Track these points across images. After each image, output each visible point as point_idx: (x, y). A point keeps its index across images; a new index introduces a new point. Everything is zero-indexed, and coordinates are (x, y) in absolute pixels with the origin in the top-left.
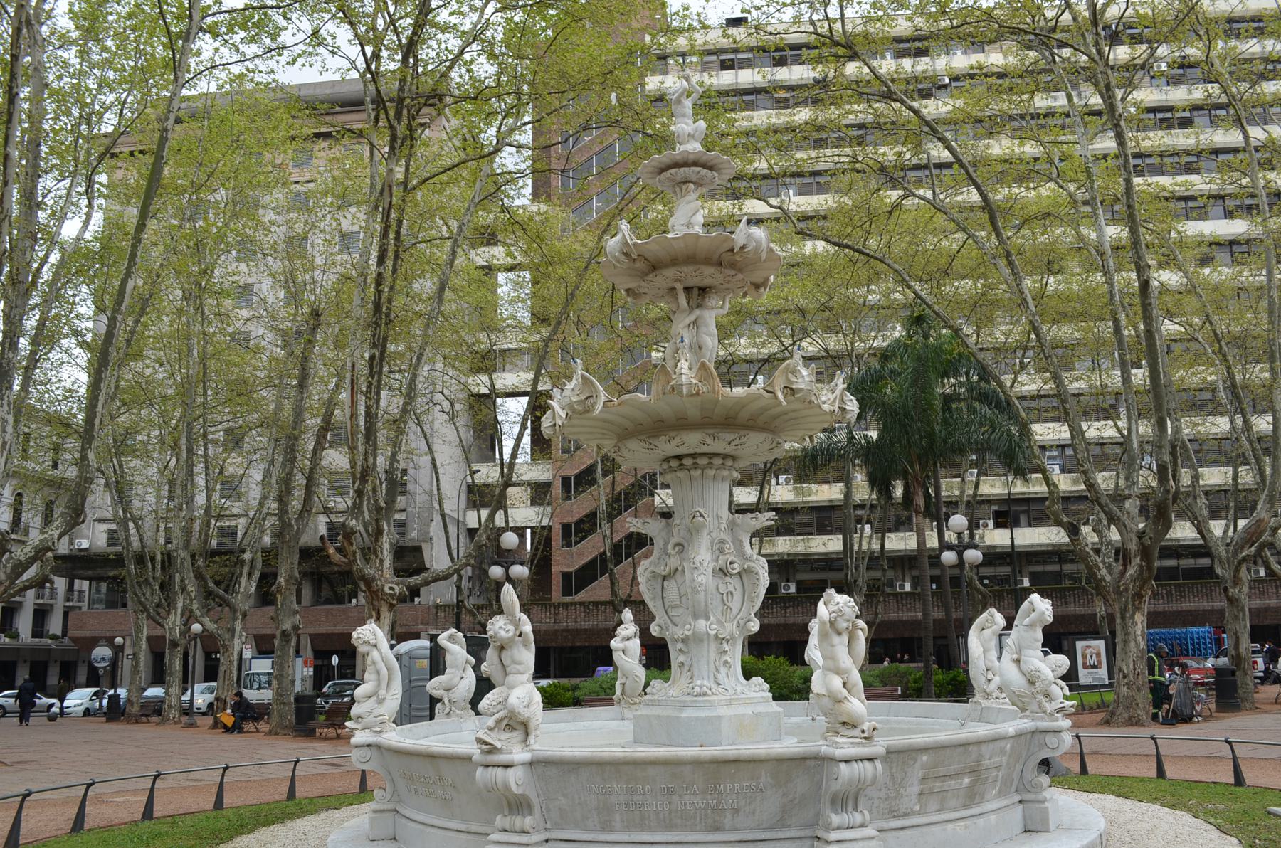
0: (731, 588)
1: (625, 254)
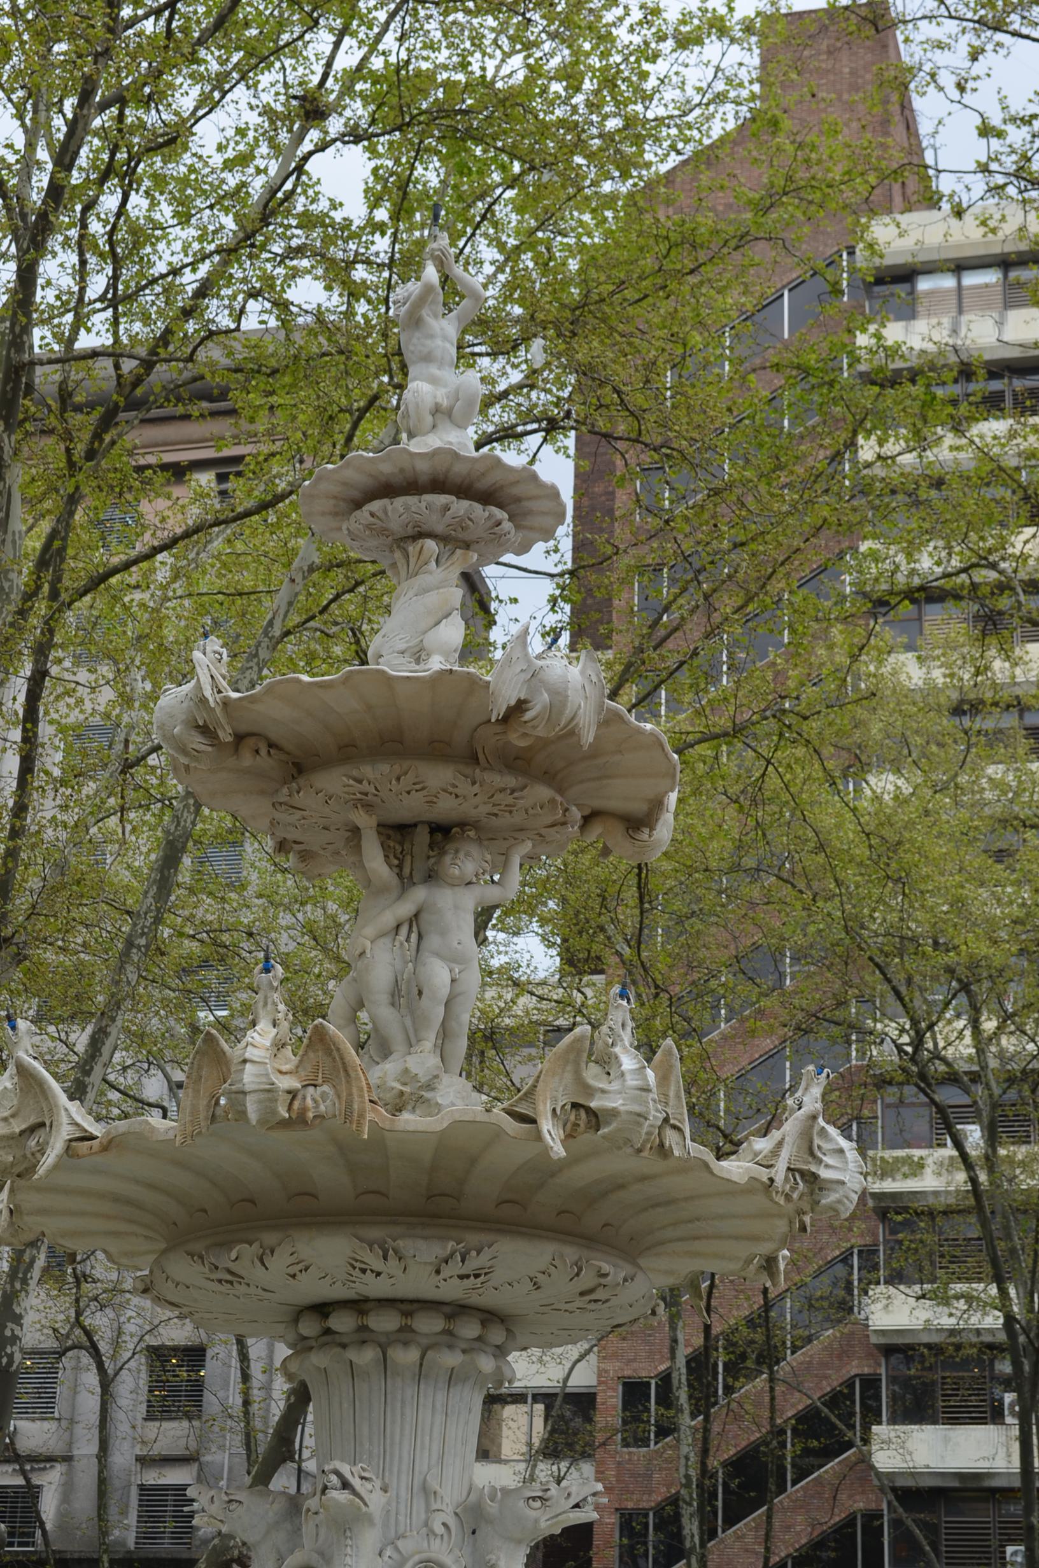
1: (205, 730)
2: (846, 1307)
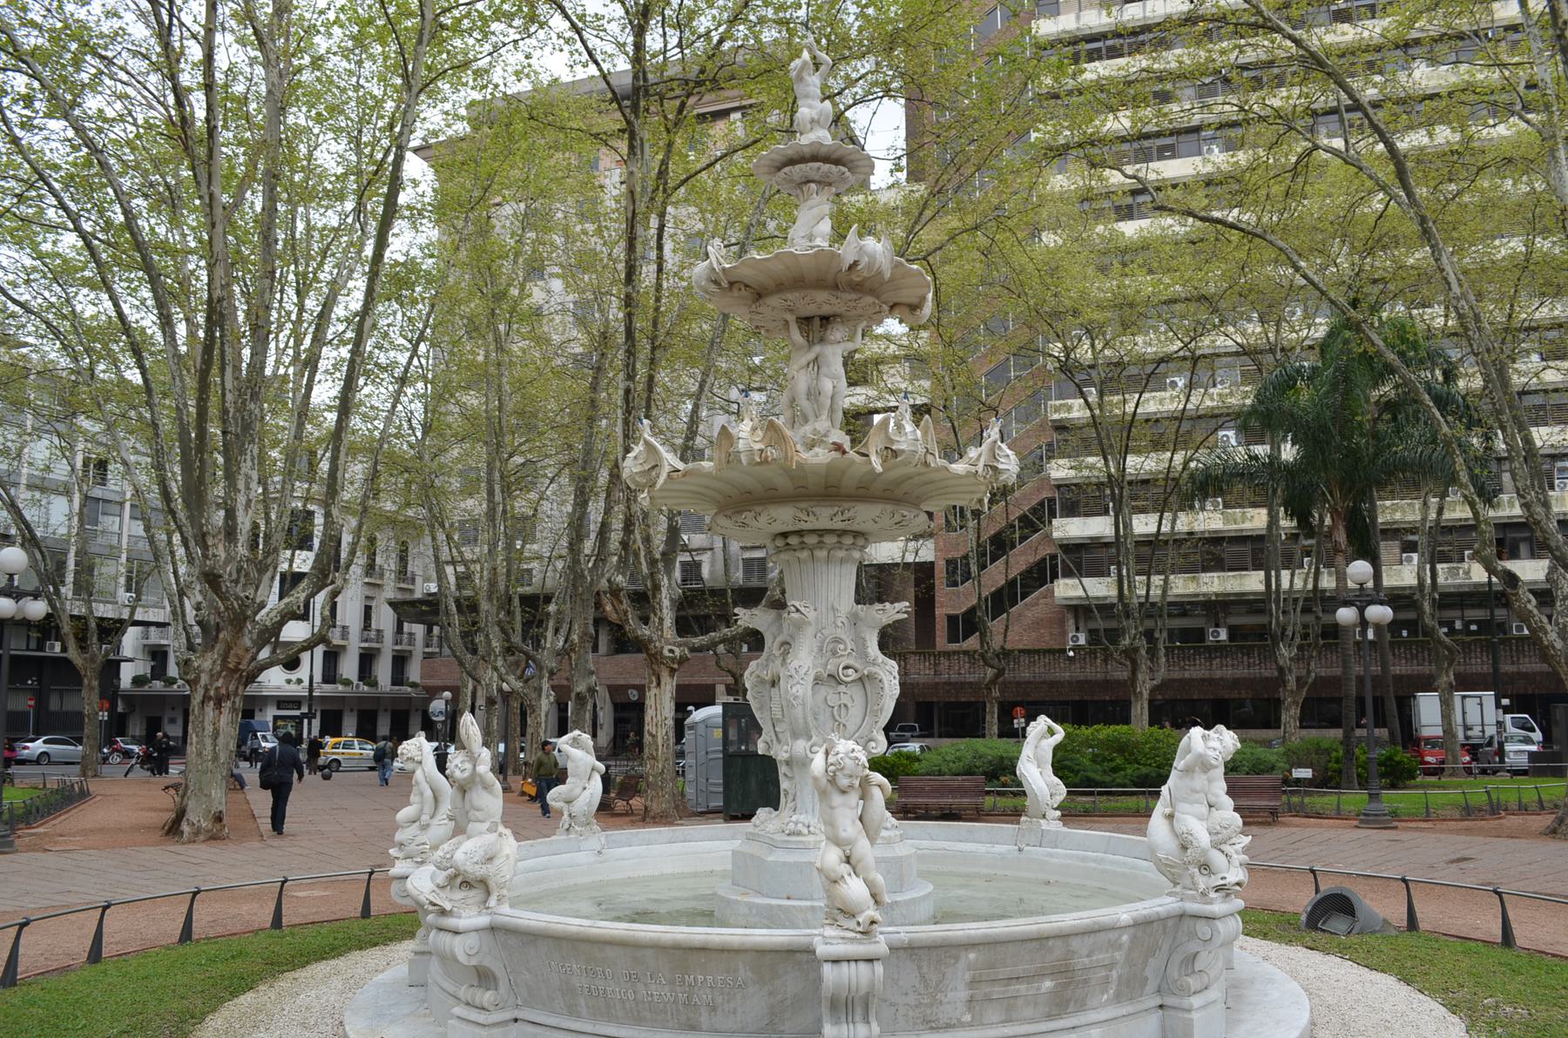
0: (845, 699)
1: (716, 282)
2: (1041, 469)
